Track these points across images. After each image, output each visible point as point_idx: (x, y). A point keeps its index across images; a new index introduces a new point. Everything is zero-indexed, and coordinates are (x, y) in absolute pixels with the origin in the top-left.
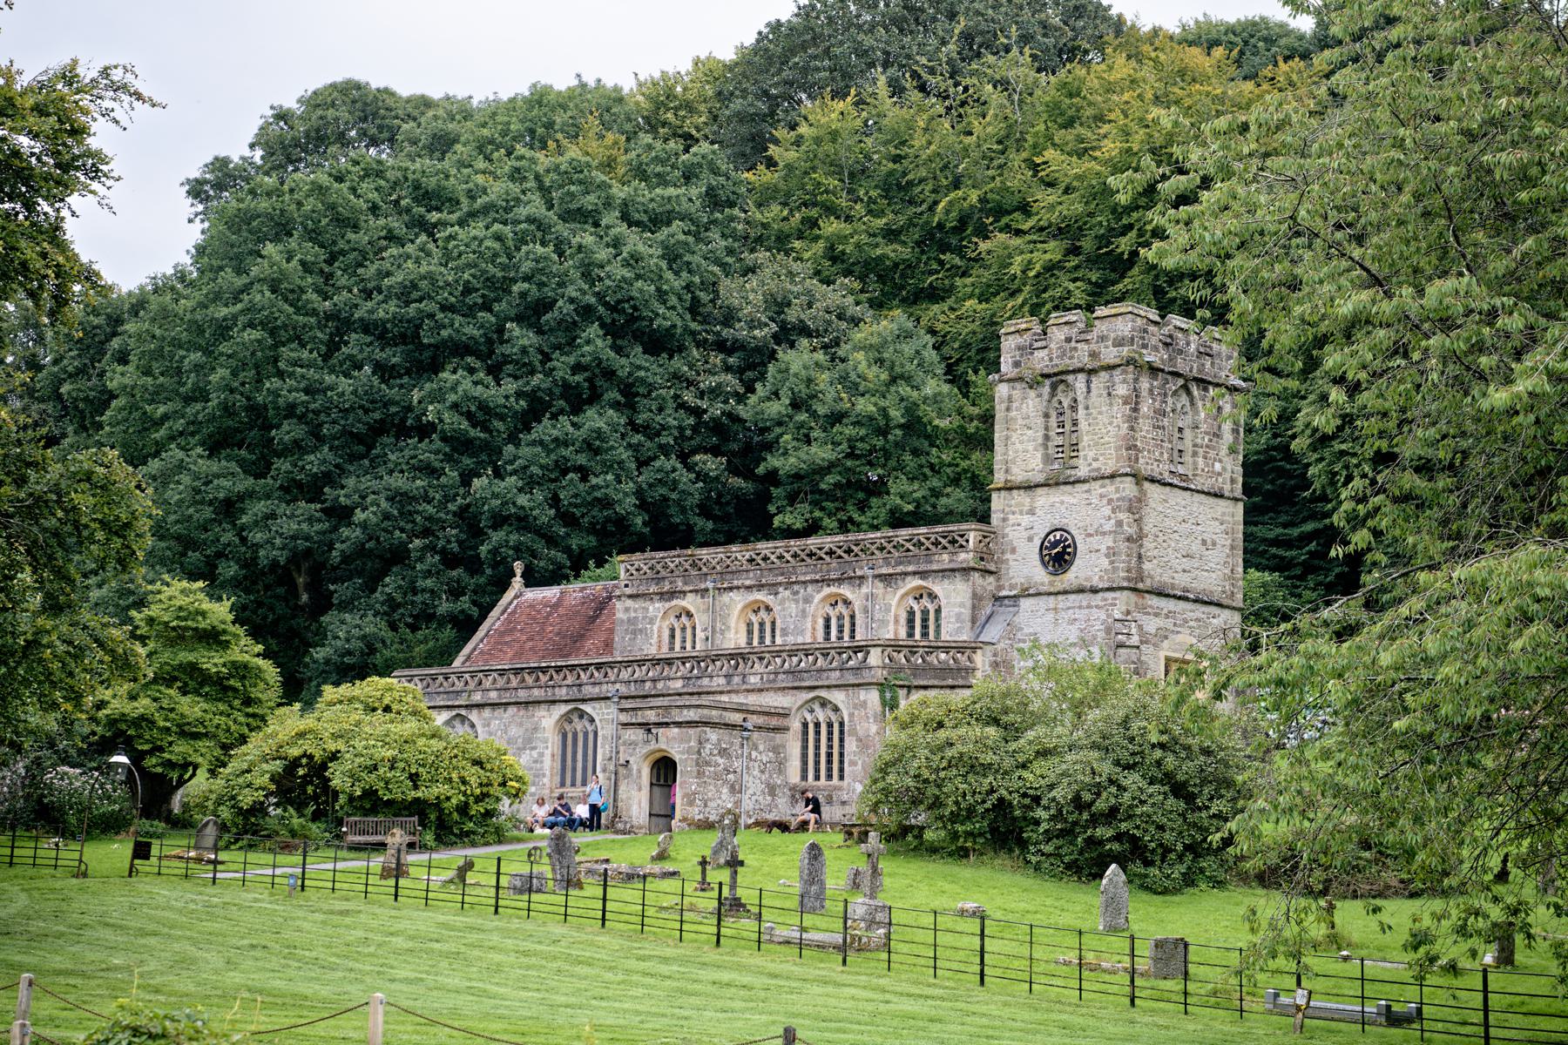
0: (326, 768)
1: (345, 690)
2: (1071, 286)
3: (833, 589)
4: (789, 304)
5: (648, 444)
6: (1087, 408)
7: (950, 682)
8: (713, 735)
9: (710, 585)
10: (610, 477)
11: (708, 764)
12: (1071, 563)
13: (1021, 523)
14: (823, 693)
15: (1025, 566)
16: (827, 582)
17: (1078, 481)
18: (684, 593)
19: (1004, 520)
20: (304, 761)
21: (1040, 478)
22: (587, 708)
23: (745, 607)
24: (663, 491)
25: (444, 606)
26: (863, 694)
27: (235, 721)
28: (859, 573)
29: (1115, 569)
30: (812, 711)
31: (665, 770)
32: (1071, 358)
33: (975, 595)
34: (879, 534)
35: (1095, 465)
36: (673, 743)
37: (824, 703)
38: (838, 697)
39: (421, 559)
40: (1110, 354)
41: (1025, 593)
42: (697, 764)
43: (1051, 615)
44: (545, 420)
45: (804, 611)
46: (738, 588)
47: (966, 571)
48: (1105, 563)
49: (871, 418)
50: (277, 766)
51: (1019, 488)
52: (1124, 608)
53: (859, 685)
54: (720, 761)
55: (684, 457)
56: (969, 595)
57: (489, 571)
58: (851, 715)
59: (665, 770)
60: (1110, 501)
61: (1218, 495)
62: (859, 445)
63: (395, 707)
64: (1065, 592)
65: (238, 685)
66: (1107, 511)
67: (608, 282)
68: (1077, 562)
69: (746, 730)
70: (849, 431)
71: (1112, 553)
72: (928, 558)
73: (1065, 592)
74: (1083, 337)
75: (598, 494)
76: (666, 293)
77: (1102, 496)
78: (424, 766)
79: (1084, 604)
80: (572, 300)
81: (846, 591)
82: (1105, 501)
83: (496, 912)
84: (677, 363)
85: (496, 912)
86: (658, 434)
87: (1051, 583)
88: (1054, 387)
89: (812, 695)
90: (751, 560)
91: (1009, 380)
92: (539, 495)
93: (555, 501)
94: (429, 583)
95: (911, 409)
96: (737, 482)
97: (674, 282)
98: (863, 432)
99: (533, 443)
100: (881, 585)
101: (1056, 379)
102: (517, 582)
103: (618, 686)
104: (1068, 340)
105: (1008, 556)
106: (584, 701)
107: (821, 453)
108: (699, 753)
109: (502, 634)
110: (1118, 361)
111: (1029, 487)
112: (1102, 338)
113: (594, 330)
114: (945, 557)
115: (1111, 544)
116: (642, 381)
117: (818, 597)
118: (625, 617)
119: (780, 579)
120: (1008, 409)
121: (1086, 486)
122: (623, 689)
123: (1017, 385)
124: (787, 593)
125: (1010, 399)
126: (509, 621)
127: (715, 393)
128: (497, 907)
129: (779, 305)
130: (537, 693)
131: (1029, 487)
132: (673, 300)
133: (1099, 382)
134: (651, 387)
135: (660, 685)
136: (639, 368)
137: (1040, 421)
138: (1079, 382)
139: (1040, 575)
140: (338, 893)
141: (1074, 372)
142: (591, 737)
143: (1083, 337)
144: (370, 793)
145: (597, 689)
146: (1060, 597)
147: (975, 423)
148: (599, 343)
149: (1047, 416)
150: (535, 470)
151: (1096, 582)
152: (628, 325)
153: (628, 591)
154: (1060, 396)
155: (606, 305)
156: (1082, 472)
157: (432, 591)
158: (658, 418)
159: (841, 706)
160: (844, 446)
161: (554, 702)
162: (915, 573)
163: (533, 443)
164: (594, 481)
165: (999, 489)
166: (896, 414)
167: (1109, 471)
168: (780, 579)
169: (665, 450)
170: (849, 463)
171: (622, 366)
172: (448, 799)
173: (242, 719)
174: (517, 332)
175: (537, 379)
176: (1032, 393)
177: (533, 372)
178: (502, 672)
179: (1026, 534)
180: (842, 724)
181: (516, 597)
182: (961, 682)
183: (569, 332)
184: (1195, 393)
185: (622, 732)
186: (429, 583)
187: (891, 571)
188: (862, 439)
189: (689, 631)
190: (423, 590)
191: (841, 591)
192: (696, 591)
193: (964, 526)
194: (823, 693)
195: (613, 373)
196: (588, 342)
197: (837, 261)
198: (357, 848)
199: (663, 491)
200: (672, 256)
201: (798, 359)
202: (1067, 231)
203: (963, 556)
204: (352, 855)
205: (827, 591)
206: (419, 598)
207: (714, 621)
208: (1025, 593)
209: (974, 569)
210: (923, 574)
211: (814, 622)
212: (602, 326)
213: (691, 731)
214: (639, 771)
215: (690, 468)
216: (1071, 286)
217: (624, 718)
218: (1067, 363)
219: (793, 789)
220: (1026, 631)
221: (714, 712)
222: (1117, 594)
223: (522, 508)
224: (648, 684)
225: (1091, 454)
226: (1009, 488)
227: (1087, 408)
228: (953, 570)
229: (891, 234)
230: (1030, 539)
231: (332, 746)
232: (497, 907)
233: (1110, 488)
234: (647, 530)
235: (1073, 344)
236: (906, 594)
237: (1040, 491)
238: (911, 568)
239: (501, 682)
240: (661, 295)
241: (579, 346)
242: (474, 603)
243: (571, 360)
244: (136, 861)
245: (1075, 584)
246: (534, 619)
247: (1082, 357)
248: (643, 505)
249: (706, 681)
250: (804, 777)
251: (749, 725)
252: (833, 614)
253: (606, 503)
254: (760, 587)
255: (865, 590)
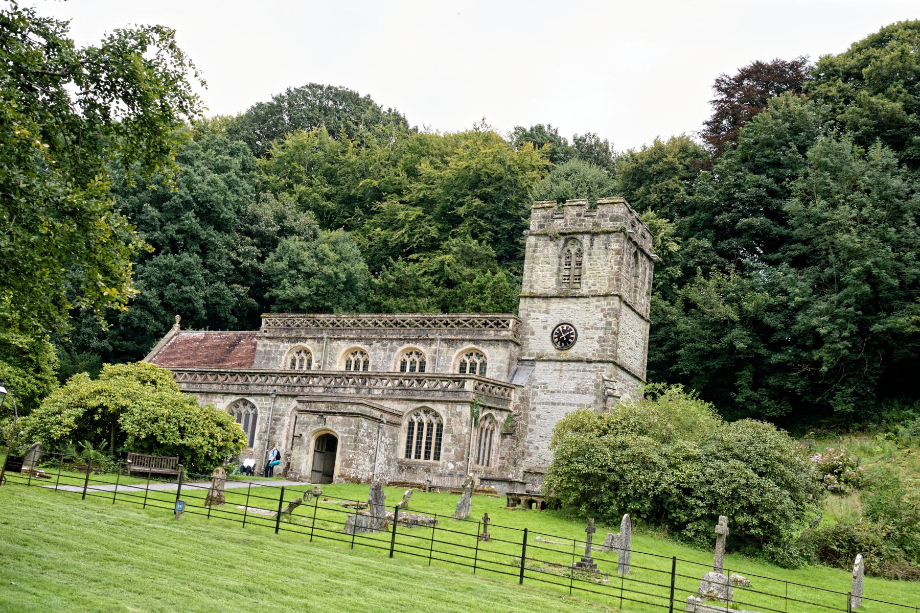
0: (118, 417)
1: (119, 367)
2: (429, 228)
3: (411, 345)
4: (285, 218)
5: (211, 275)
6: (590, 255)
7: (500, 406)
8: (365, 423)
9: (325, 335)
10: (193, 288)
11: (361, 441)
12: (573, 344)
13: (539, 321)
14: (429, 405)
15: (540, 342)
16: (409, 341)
17: (582, 297)
18: (306, 339)
19: (528, 315)
20: (100, 410)
21: (554, 293)
22: (252, 400)
23: (348, 351)
24: (217, 299)
25: (95, 343)
26: (459, 408)
27: (29, 382)
28: (431, 337)
29: (604, 350)
30: (417, 415)
31: (327, 445)
32: (581, 225)
33: (511, 358)
34: (446, 315)
35: (593, 288)
36: (336, 426)
37: (427, 411)
38: (440, 408)
39: (85, 317)
40: (607, 225)
41: (540, 359)
42: (355, 441)
43: (557, 374)
44: (161, 255)
45: (389, 356)
46: (344, 339)
47: (506, 342)
48: (597, 346)
49: (330, 277)
50: (80, 412)
51: (539, 297)
52: (609, 374)
53: (456, 402)
54: (367, 440)
55: (228, 284)
56: (507, 356)
57: (122, 328)
58: (449, 420)
59: (327, 445)
60: (603, 310)
61: (642, 317)
62: (321, 289)
63: (159, 381)
64: (569, 361)
65: (34, 358)
66: (601, 316)
67: (200, 191)
68: (577, 344)
69: (382, 422)
70: (317, 281)
71: (602, 341)
72: (480, 332)
73: (569, 361)
74: (589, 214)
75: (185, 295)
76: (228, 202)
77: (597, 307)
78: (189, 423)
79: (581, 369)
80: (181, 197)
81: (420, 347)
82: (599, 310)
83: (391, 556)
84: (228, 237)
85: (391, 556)
86: (216, 271)
87: (558, 355)
88: (566, 241)
89: (420, 405)
90: (354, 324)
91: (536, 235)
92: (154, 291)
93: (161, 296)
94: (88, 330)
95: (350, 276)
96: (252, 301)
97: (233, 198)
98: (323, 283)
99: (155, 265)
100: (445, 345)
101: (570, 237)
102: (177, 326)
103: (275, 388)
104: (579, 215)
105: (529, 336)
106: (250, 395)
107: (303, 290)
108: (357, 433)
109: (168, 354)
110: (614, 229)
111: (546, 297)
112: (603, 216)
113: (191, 214)
114: (492, 332)
115: (602, 335)
116: (213, 243)
117: (400, 349)
118: (263, 350)
119: (374, 336)
120: (534, 251)
121: (586, 300)
122: (279, 390)
123: (541, 238)
124: (379, 345)
125: (536, 246)
126: (171, 347)
127: (246, 255)
128: (392, 551)
129: (280, 218)
130: (215, 387)
131: (546, 297)
132: (231, 206)
133: (599, 241)
134: (216, 247)
135: (306, 390)
136: (212, 236)
137: (556, 260)
138: (586, 240)
139: (550, 349)
140: (212, 520)
141: (583, 233)
142: (251, 417)
143: (589, 214)
144: (151, 438)
145: (260, 389)
146: (564, 364)
147: (392, 283)
148: (193, 220)
149: (560, 257)
150: (154, 279)
151: (590, 356)
152: (207, 213)
153: (267, 335)
154: (569, 247)
155: (197, 202)
156: (584, 291)
157: (89, 335)
158: (218, 263)
159: (442, 414)
160: (314, 288)
161: (227, 394)
162: (470, 340)
163: (155, 265)
164: (184, 288)
165: (525, 297)
166: (343, 276)
167: (603, 293)
168: (374, 336)
169: (220, 278)
170: (315, 298)
171: (203, 234)
172: (202, 447)
173: (34, 381)
174: (150, 208)
175: (156, 234)
176: (552, 244)
177: (155, 230)
178: (191, 373)
179: (542, 325)
180: (440, 426)
181: (175, 335)
182: (504, 407)
183: (176, 214)
184: (639, 257)
185: (299, 415)
186: (88, 330)
187: (454, 337)
188: (323, 287)
189: (305, 362)
190: (84, 334)
191: (417, 347)
192: (314, 339)
193: (507, 315)
194: (429, 405)
195: (198, 236)
196: (187, 218)
197: (303, 205)
198: (135, 474)
199: (217, 299)
200: (230, 184)
201: (292, 243)
202: (425, 203)
203: (504, 333)
204: (133, 479)
205: (406, 346)
206: (81, 338)
207: (325, 357)
208: (540, 359)
209: (512, 341)
210: (476, 341)
211: (396, 363)
212: (195, 212)
213: (352, 420)
214: (309, 442)
215: (232, 289)
216: (429, 228)
217: (301, 407)
218: (577, 228)
219: (401, 463)
220: (539, 381)
221: (368, 409)
222: (605, 365)
223: (145, 297)
224: (297, 389)
225: (591, 282)
226: (532, 297)
227: (590, 255)
228: (497, 341)
229: (328, 197)
230: (545, 328)
231: (123, 402)
232: (392, 551)
233: (603, 302)
234: (206, 318)
235: (582, 217)
236: (462, 352)
237: (553, 300)
238: (467, 337)
239: (190, 378)
240: (225, 202)
241: (182, 220)
242: (110, 343)
243: (176, 227)
244: (6, 473)
245: (575, 356)
246: (188, 347)
247: (588, 224)
248: (206, 306)
249: (341, 390)
250: (408, 455)
251: (383, 419)
252: (408, 360)
253: (189, 300)
254: (360, 340)
255: (433, 347)
